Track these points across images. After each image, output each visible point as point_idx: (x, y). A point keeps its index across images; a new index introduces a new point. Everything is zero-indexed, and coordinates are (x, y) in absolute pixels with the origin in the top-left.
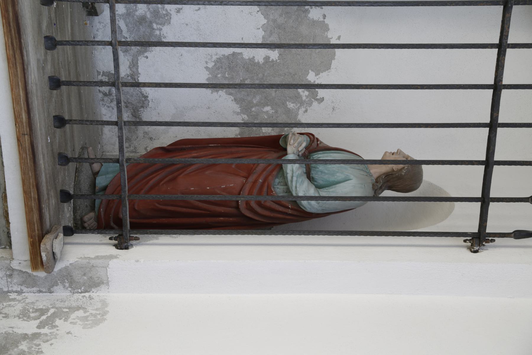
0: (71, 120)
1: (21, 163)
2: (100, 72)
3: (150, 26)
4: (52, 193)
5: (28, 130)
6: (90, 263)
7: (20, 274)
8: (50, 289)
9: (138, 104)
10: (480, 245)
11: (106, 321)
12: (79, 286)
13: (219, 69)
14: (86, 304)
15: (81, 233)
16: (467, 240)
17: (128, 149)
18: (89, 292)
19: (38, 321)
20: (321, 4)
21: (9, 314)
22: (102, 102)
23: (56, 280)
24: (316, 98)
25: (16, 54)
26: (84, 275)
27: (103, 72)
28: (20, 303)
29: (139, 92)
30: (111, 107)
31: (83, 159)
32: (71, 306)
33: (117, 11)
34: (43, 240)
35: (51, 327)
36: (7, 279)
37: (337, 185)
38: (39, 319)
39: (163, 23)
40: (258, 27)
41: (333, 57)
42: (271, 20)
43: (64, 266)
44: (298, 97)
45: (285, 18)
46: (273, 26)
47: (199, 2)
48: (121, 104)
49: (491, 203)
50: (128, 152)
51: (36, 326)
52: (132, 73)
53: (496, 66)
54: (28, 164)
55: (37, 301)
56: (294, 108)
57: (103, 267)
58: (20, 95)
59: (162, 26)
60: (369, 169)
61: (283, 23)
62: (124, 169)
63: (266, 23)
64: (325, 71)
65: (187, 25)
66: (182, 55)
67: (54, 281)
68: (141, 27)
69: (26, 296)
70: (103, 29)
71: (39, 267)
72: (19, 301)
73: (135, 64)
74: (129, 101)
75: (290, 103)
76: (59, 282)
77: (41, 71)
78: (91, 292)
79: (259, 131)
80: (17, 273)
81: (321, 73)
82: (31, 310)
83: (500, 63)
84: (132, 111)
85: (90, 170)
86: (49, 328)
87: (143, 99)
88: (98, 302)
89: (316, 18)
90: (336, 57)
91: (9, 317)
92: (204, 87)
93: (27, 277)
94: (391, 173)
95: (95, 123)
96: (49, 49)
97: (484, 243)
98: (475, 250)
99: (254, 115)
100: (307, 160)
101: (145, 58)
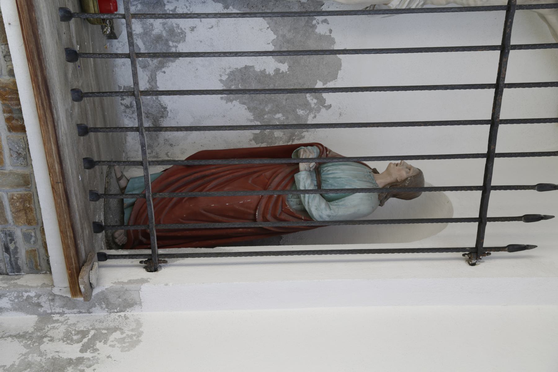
0: (99, 162)
1: (56, 208)
2: (121, 87)
3: (166, 43)
4: (86, 225)
5: (61, 178)
6: (124, 288)
7: (61, 298)
8: (89, 310)
9: (158, 115)
10: (478, 259)
11: (141, 342)
12: (115, 307)
13: (233, 81)
14: (122, 324)
15: (114, 259)
16: (465, 254)
17: (151, 155)
18: (124, 311)
19: (80, 344)
20: (330, 53)
21: (54, 337)
22: (125, 113)
23: (94, 302)
24: (324, 105)
25: (46, 113)
26: (119, 297)
27: (124, 86)
28: (63, 324)
29: (158, 104)
30: (133, 118)
31: (113, 196)
32: (108, 327)
33: (135, 31)
34: (80, 273)
35: (93, 350)
36: (50, 303)
37: (346, 198)
38: (81, 342)
39: (179, 40)
40: (268, 42)
41: (339, 66)
42: (280, 35)
43: (100, 290)
44: (306, 105)
45: (293, 33)
46: (283, 41)
47: (215, 55)
48: (145, 148)
49: (488, 223)
50: (150, 157)
51: (79, 350)
52: (150, 87)
53: (493, 104)
54: (63, 208)
55: (78, 322)
56: (303, 114)
57: (136, 290)
58: (52, 149)
59: (178, 44)
60: (375, 179)
61: (292, 38)
62: (151, 203)
63: (275, 38)
64: (332, 80)
65: (201, 42)
66: (197, 70)
67: (92, 303)
68: (158, 45)
69: (68, 317)
70: (122, 48)
71: (78, 294)
72: (62, 322)
73: (154, 78)
74: (150, 112)
75: (300, 110)
76: (96, 304)
77: (70, 119)
78: (126, 311)
79: (272, 135)
80: (58, 297)
81: (328, 83)
82: (73, 332)
83: (497, 102)
84: (153, 121)
85: (118, 186)
86: (91, 352)
87: (163, 110)
88: (133, 321)
89: (322, 33)
90: (342, 68)
91: (54, 340)
92: (222, 129)
93: (68, 301)
94: (395, 184)
95: (122, 164)
96: (76, 101)
97: (481, 257)
98: (472, 263)
99: (267, 121)
100: (319, 191)
101: (163, 74)
